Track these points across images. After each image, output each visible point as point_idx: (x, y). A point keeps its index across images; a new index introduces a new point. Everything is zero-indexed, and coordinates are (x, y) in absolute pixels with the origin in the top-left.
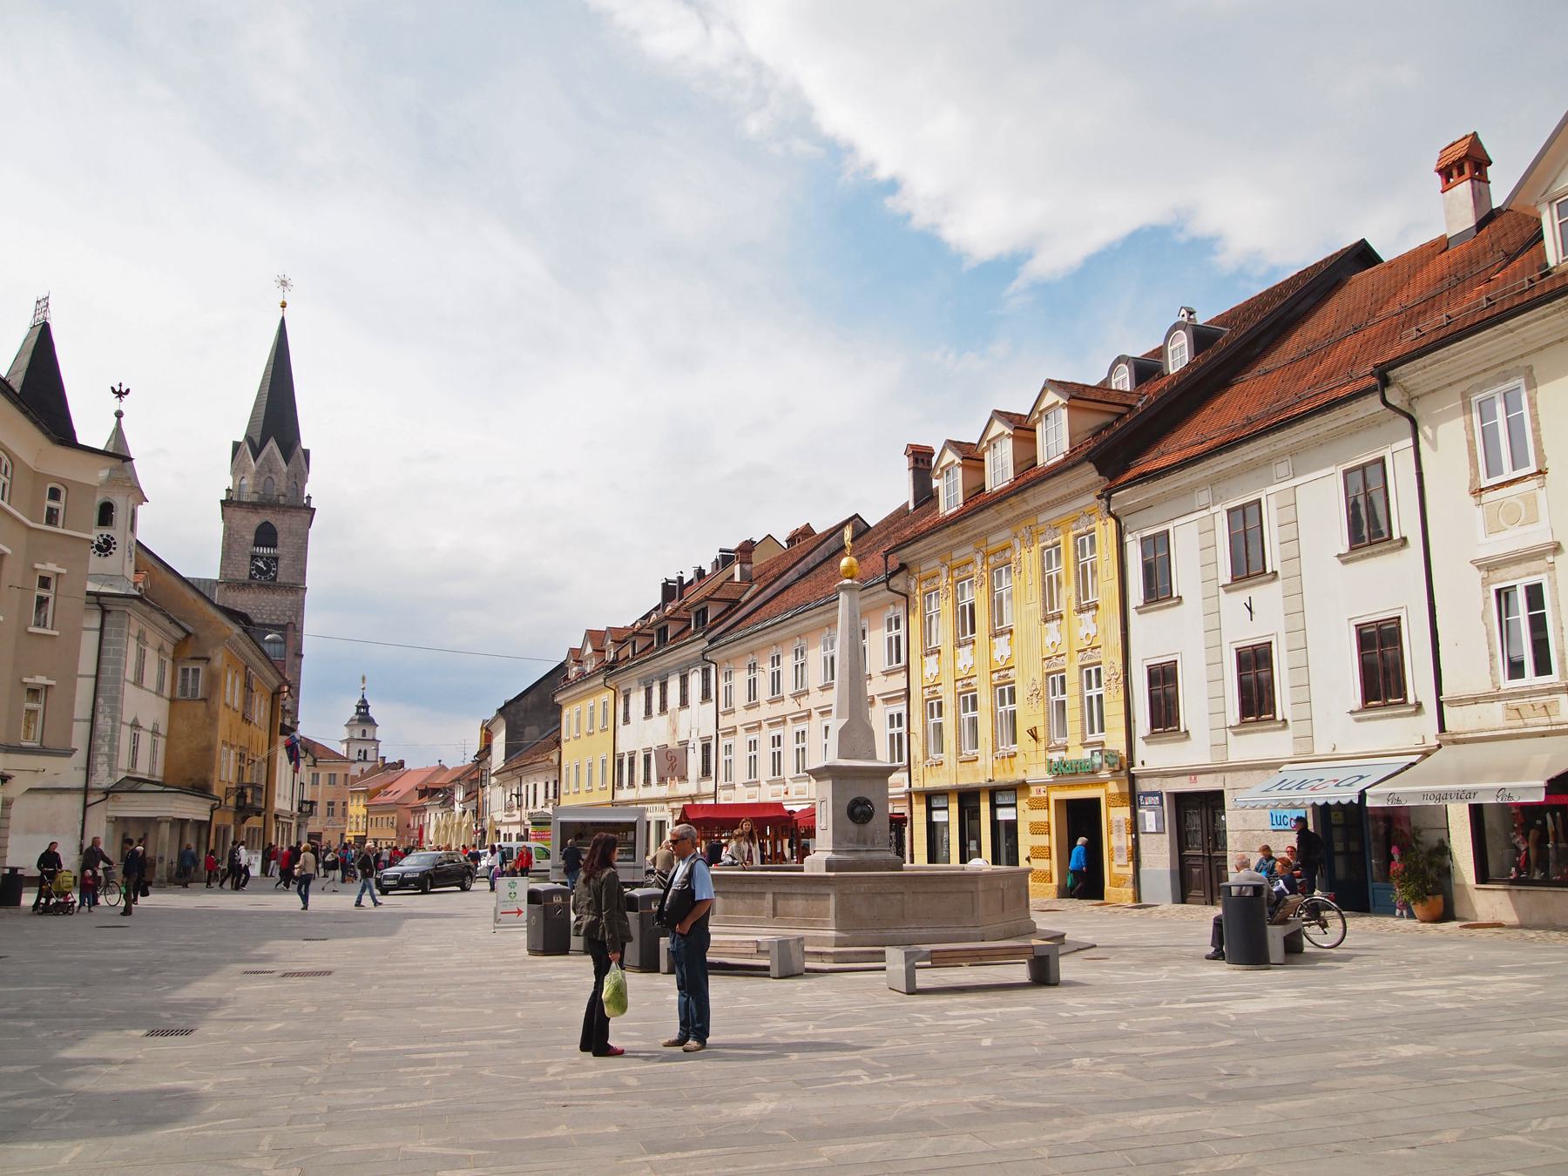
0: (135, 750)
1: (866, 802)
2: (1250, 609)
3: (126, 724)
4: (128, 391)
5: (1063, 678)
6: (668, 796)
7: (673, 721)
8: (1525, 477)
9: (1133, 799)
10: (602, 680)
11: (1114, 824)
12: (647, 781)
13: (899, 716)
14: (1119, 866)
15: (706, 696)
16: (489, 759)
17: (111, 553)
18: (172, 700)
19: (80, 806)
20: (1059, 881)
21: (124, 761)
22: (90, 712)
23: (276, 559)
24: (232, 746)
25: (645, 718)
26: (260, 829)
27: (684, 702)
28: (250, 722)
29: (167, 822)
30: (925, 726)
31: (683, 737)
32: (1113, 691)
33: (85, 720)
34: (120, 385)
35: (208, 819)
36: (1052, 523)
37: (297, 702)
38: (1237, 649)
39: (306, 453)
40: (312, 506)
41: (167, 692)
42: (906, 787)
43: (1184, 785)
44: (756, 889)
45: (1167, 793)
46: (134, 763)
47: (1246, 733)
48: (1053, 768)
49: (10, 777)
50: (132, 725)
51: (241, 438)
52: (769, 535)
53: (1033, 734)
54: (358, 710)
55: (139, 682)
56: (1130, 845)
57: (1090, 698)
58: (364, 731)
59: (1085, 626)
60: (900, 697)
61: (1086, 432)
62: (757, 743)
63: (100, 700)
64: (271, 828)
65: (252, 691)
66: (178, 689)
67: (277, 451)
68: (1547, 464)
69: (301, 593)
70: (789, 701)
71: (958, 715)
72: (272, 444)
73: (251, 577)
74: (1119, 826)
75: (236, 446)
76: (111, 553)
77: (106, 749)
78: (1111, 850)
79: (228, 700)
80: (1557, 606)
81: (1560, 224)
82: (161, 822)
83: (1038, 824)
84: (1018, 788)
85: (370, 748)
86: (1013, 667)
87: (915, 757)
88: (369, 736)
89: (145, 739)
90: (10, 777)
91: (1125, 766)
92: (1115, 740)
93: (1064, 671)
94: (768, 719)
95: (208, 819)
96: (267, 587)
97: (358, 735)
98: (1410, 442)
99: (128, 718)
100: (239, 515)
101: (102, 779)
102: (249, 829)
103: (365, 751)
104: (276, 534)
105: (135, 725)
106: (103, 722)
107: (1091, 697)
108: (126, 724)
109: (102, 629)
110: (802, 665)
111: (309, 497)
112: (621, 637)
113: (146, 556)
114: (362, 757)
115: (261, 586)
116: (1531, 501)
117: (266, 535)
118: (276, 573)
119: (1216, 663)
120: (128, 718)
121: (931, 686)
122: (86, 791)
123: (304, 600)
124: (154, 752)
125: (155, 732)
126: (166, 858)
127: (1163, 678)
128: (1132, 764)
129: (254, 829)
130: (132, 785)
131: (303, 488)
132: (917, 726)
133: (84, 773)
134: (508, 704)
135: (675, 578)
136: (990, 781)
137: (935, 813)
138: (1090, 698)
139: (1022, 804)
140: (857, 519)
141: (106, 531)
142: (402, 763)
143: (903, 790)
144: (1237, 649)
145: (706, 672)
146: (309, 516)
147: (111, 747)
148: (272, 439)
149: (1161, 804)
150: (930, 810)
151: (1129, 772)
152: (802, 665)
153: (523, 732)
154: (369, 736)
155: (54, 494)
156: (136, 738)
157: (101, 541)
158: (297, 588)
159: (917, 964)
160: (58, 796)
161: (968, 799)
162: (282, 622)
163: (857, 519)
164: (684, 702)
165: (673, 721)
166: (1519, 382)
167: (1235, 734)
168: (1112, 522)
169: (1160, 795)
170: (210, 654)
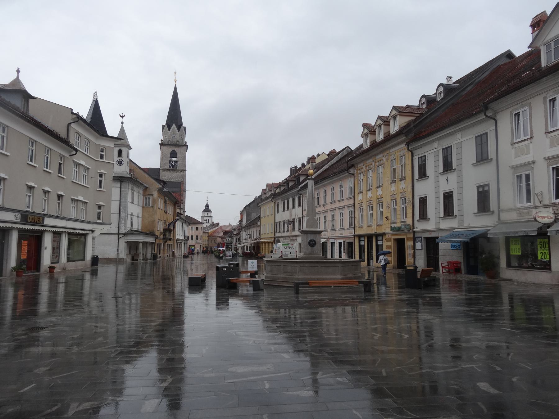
0: (132, 222)
1: (314, 241)
2: (448, 181)
3: (129, 214)
4: (124, 115)
5: (396, 201)
6: (289, 235)
7: (291, 213)
8: (527, 139)
9: (415, 240)
10: (271, 200)
11: (408, 247)
12: (284, 231)
13: (352, 212)
14: (410, 259)
15: (299, 205)
16: (242, 223)
17: (122, 165)
18: (143, 207)
19: (117, 238)
20: (394, 263)
21: (129, 225)
22: (119, 211)
23: (177, 162)
24: (161, 220)
25: (283, 211)
26: (172, 244)
27: (294, 207)
28: (167, 213)
29: (141, 242)
30: (359, 216)
31: (293, 217)
32: (409, 206)
33: (117, 213)
34: (122, 114)
35: (154, 241)
36: (403, 148)
37: (185, 206)
38: (443, 193)
39: (185, 128)
40: (187, 145)
41: (141, 205)
42: (353, 234)
43: (428, 235)
44: (279, 264)
45: (424, 237)
46: (132, 225)
47: (445, 219)
48: (393, 229)
49: (94, 231)
50: (131, 215)
51: (164, 124)
52: (324, 152)
53: (387, 218)
54: (206, 207)
55: (132, 203)
56: (413, 253)
57: (403, 207)
58: (208, 214)
59: (402, 185)
60: (351, 206)
61: (405, 123)
62: (327, 217)
63: (121, 208)
64: (175, 244)
65: (167, 204)
66: (145, 204)
67: (175, 127)
68: (534, 135)
69: (185, 172)
70: (322, 207)
71: (367, 212)
72: (174, 127)
73: (170, 167)
74: (410, 247)
75: (163, 126)
76: (122, 165)
77: (123, 222)
78: (407, 254)
79: (159, 207)
80: (533, 181)
81: (547, 53)
82: (140, 242)
83: (389, 246)
84: (383, 234)
85: (210, 219)
86: (382, 198)
87: (356, 225)
88: (209, 215)
89: (135, 219)
90: (94, 231)
91: (412, 228)
92: (409, 221)
93: (396, 199)
94: (338, 207)
95: (154, 241)
96: (174, 170)
97: (206, 215)
98: (494, 127)
99: (130, 212)
100: (165, 148)
101: (123, 231)
102: (168, 244)
103: (208, 220)
104: (177, 154)
105: (132, 215)
106: (122, 214)
107: (403, 207)
108: (129, 214)
109: (121, 187)
110: (326, 195)
111: (186, 142)
112: (278, 186)
113: (133, 164)
114: (207, 222)
115: (172, 170)
116: (528, 146)
117: (173, 154)
118: (177, 166)
119: (437, 197)
120: (130, 212)
121: (379, 198)
122: (118, 234)
123: (186, 174)
124: (138, 222)
125: (138, 217)
126: (142, 253)
127: (423, 201)
128: (414, 228)
129: (170, 244)
130: (132, 232)
131: (184, 139)
132: (356, 216)
133: (118, 229)
134: (247, 206)
135: (294, 166)
136: (376, 232)
137: (378, 242)
138: (403, 207)
139: (384, 240)
140: (348, 148)
141: (120, 158)
142: (218, 224)
143: (352, 235)
144: (443, 193)
145: (299, 198)
146: (186, 148)
147: (125, 221)
148: (174, 124)
149: (422, 241)
150: (360, 241)
151: (413, 231)
152: (326, 195)
153: (251, 215)
154: (209, 215)
155: (102, 151)
156: (132, 218)
157: (120, 161)
158: (183, 171)
159: (299, 286)
160: (111, 235)
161: (370, 237)
162: (179, 181)
163: (348, 148)
164: (294, 207)
165: (291, 213)
166: (527, 108)
167: (442, 219)
168: (410, 153)
169: (421, 238)
170: (153, 193)
